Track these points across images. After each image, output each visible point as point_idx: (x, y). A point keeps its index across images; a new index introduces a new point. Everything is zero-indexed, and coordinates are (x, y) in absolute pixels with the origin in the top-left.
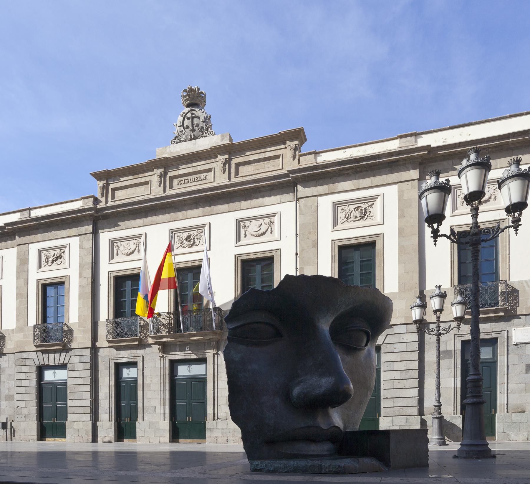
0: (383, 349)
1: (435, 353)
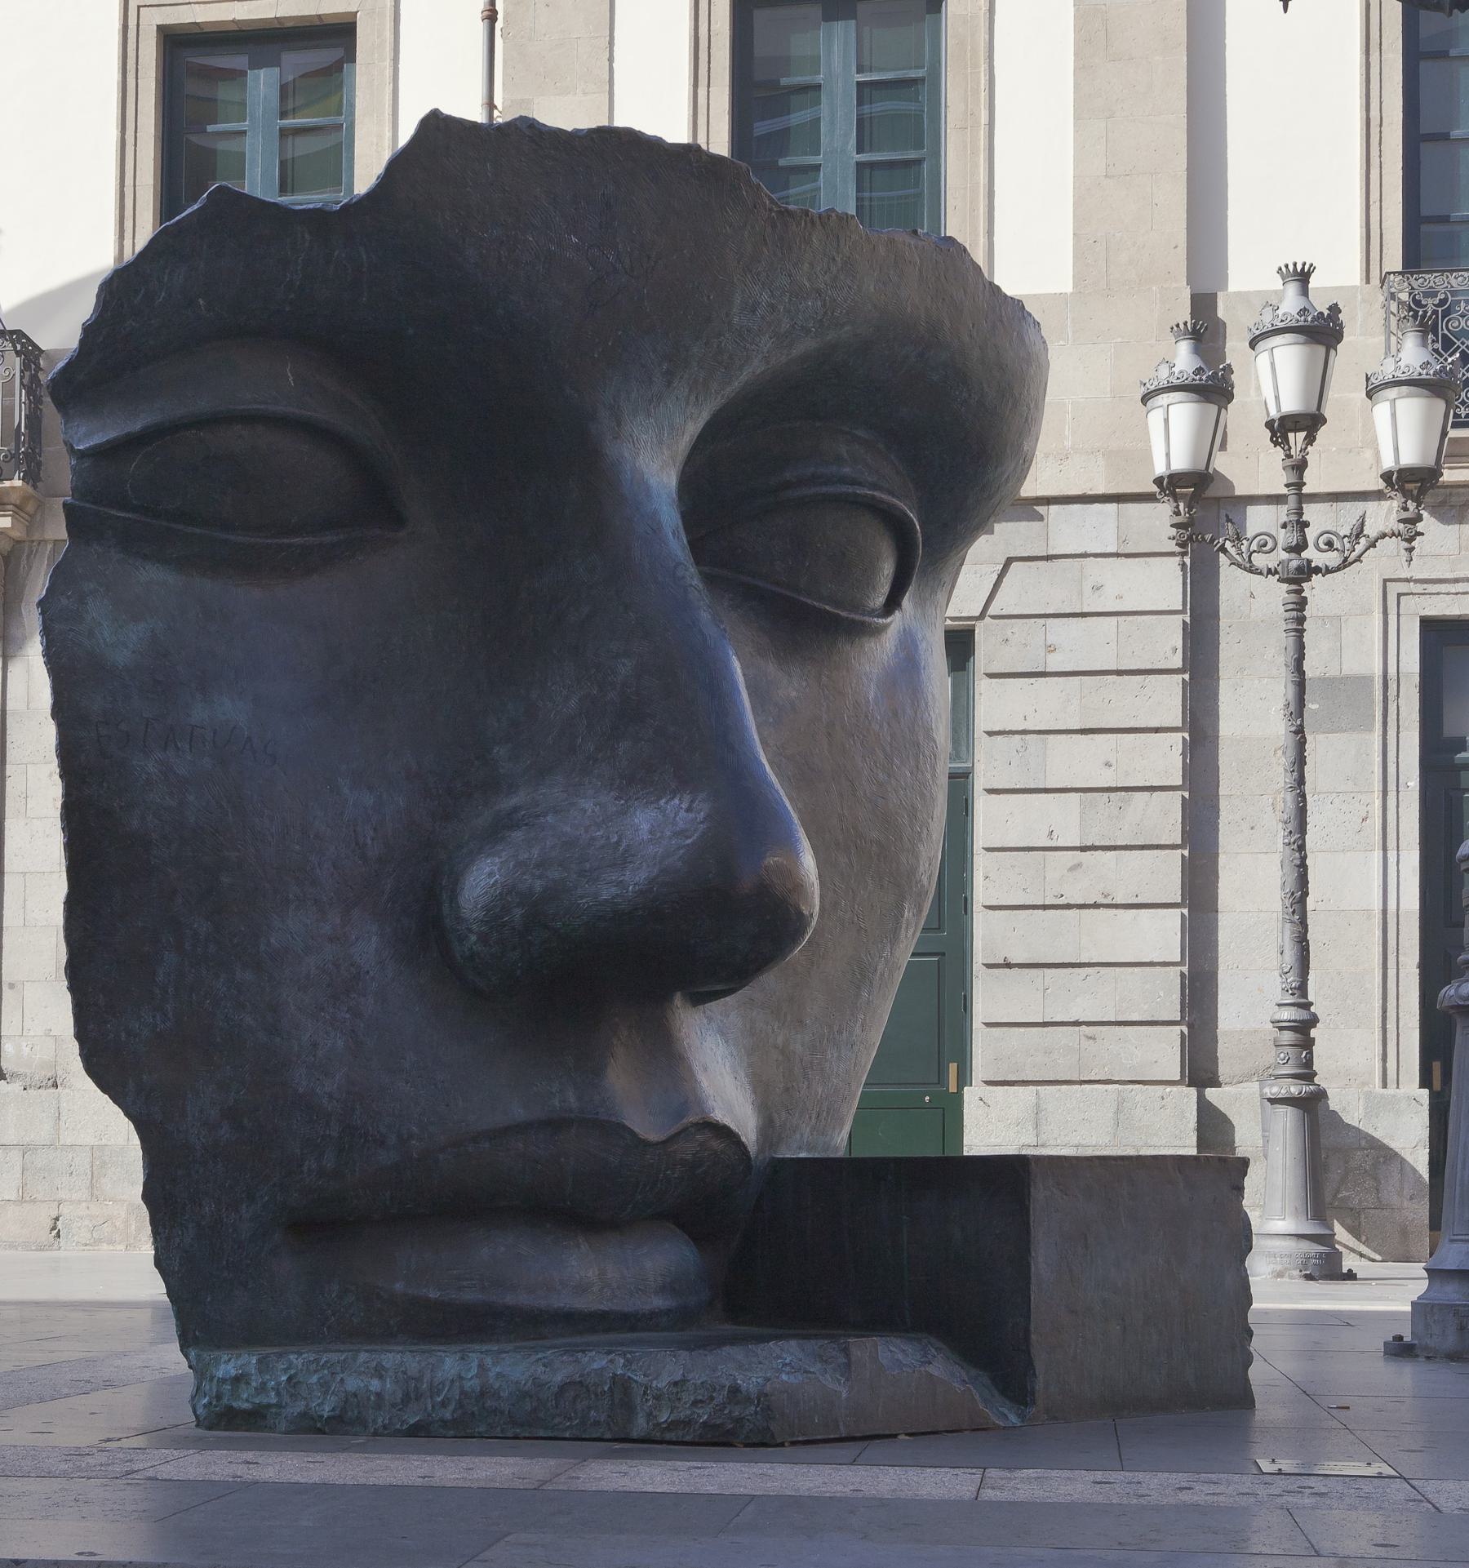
0: (987, 652)
1: (1280, 690)
